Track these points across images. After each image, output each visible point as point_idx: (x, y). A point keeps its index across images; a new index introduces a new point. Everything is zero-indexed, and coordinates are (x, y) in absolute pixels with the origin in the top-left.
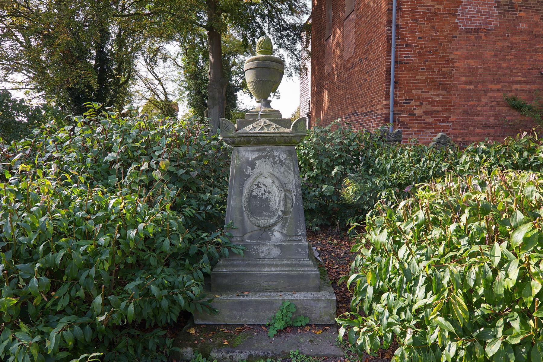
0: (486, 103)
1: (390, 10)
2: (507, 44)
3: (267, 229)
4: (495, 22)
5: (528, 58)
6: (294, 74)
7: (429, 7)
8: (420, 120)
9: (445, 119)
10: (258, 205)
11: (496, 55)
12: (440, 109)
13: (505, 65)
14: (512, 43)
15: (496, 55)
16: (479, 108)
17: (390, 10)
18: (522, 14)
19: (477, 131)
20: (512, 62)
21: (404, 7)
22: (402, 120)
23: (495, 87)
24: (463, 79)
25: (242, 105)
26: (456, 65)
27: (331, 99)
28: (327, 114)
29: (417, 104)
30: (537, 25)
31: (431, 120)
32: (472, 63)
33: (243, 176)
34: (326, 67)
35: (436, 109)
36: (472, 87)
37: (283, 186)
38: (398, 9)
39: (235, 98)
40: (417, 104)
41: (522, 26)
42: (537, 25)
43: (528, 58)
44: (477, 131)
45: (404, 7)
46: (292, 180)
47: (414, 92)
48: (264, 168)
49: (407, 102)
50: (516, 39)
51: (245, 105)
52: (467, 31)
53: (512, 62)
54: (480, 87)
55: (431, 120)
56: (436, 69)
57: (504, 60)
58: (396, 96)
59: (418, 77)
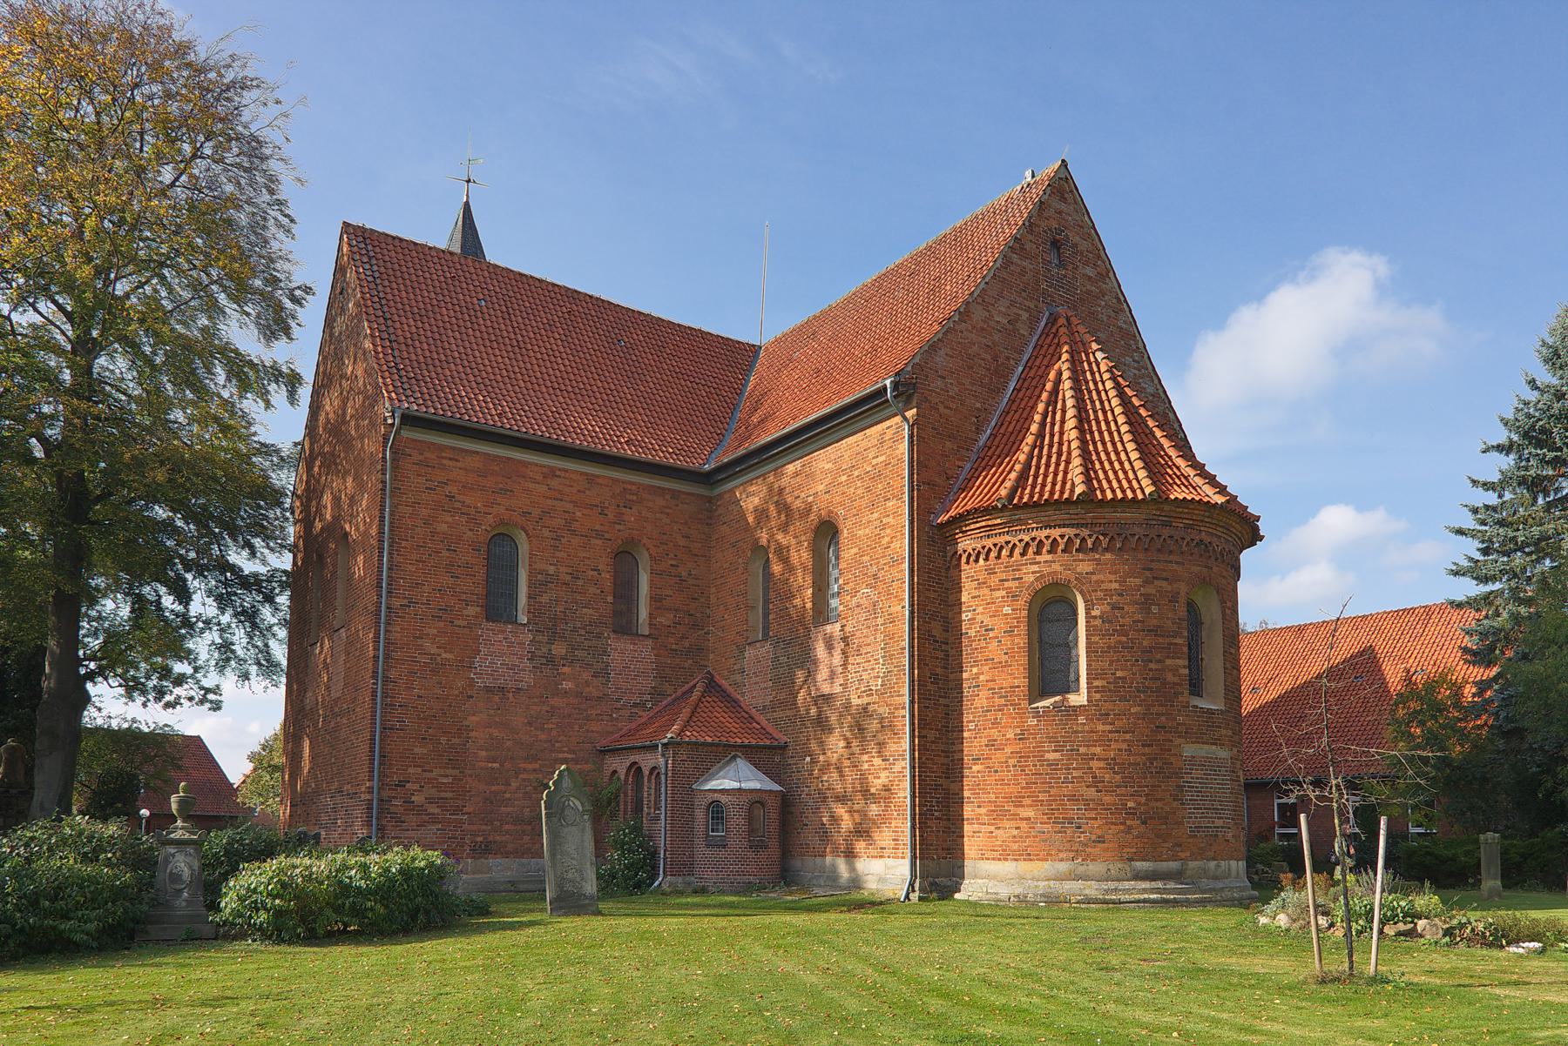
0: (518, 788)
1: (376, 658)
2: (545, 708)
3: (181, 891)
4: (528, 679)
5: (576, 728)
6: (253, 676)
7: (433, 656)
8: (420, 810)
9: (458, 810)
10: (175, 878)
11: (530, 724)
12: (449, 795)
13: (543, 737)
14: (553, 707)
15: (530, 724)
16: (507, 795)
17: (376, 658)
18: (566, 669)
19: (506, 827)
20: (554, 733)
21: (397, 655)
22: (392, 809)
23: (530, 766)
24: (483, 753)
25: (95, 714)
26: (473, 734)
27: (313, 757)
28: (306, 784)
29: (416, 787)
30: (587, 684)
31: (437, 811)
32: (496, 733)
33: (167, 861)
34: (309, 694)
35: (443, 795)
36: (496, 765)
37: (190, 867)
38: (387, 657)
39: (86, 699)
40: (416, 787)
41: (567, 685)
42: (587, 684)
43: (576, 728)
44: (506, 827)
45: (397, 655)
46: (196, 865)
47: (411, 770)
48: (180, 857)
49: (401, 784)
50: (558, 702)
51: (104, 713)
52: (488, 689)
53: (554, 733)
54: (507, 765)
55: (437, 811)
56: (443, 740)
57: (542, 729)
58: (382, 775)
59: (416, 750)
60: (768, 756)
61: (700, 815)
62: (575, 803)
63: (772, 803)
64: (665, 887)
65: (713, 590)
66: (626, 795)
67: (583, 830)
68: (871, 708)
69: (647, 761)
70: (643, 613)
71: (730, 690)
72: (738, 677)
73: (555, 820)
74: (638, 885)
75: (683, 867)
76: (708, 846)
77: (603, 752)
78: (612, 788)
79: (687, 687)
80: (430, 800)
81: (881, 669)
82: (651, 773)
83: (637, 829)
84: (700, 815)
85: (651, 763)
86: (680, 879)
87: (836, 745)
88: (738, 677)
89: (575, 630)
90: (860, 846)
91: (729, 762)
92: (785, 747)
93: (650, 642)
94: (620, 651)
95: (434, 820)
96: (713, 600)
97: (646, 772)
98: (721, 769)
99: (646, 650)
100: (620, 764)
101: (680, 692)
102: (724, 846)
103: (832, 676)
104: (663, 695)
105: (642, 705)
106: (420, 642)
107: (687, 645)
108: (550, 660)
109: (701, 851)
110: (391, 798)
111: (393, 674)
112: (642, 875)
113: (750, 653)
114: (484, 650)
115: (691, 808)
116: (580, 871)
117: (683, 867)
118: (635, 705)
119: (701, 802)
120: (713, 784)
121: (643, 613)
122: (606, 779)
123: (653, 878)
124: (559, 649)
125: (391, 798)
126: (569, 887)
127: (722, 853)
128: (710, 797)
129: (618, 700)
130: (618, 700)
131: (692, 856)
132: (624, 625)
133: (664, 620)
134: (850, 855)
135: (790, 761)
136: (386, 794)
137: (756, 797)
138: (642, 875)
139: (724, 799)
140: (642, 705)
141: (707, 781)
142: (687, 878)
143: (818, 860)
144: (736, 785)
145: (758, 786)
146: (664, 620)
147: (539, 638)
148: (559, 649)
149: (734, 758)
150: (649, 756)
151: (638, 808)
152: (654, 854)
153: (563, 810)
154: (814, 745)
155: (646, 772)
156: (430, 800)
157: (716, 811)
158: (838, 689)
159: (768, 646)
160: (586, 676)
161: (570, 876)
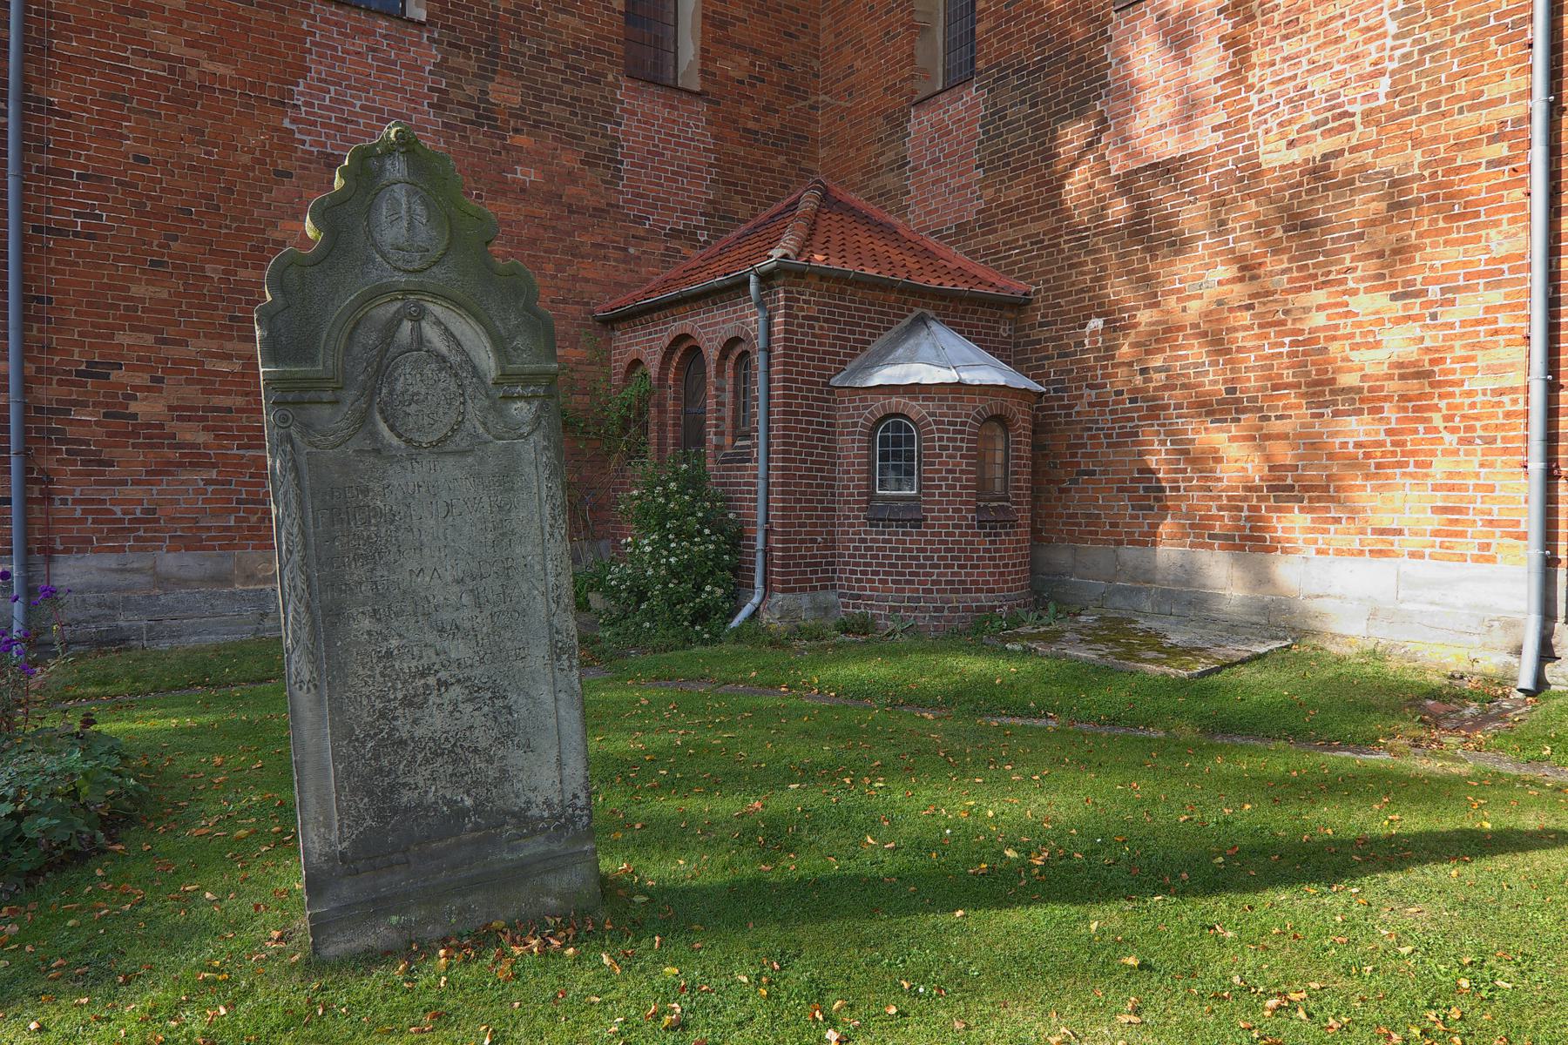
8: (154, 435)
18: (522, 140)
29: (142, 379)
30: (571, 177)
31: (202, 438)
35: (218, 400)
40: (142, 379)
41: (525, 174)
43: (550, 268)
47: (124, 338)
49: (95, 372)
55: (202, 438)
56: (213, 270)
59: (136, 290)
60: (985, 316)
61: (851, 449)
62: (457, 331)
63: (1022, 419)
64: (771, 619)
65: (825, 21)
66: (662, 410)
67: (507, 477)
68: (1340, 165)
69: (711, 329)
70: (689, 51)
71: (872, 208)
72: (890, 180)
73: (332, 418)
74: (701, 616)
75: (808, 569)
76: (873, 521)
77: (613, 322)
78: (631, 392)
79: (776, 207)
80: (183, 412)
81: (1390, 50)
82: (724, 355)
83: (694, 482)
84: (851, 449)
85: (728, 330)
86: (805, 600)
87: (1201, 279)
88: (890, 180)
89: (540, 56)
90: (1293, 523)
91: (910, 331)
92: (1019, 305)
93: (702, 107)
94: (639, 115)
95: (196, 458)
96: (827, 39)
97: (712, 353)
98: (895, 344)
99: (695, 124)
100: (646, 346)
101: (763, 215)
102: (918, 523)
103: (1189, 110)
104: (730, 218)
105: (689, 235)
106: (135, 23)
107: (776, 122)
108: (485, 115)
109: (854, 533)
110: (63, 409)
111: (57, 94)
112: (713, 591)
113: (920, 123)
114: (316, 69)
115: (827, 431)
116: (492, 693)
117: (808, 569)
118: (675, 234)
119: (852, 420)
120: (884, 376)
121: (689, 51)
122: (617, 380)
123: (735, 599)
124: (505, 94)
125: (63, 409)
126: (429, 786)
127: (912, 539)
128: (879, 405)
129: (640, 220)
130: (640, 220)
131: (830, 544)
132: (648, 62)
133: (733, 67)
134: (1251, 541)
135: (1036, 334)
136: (49, 393)
137: (992, 405)
138: (713, 591)
139: (916, 408)
140: (689, 235)
141: (880, 360)
142: (821, 596)
143: (1129, 553)
144: (949, 376)
145: (1000, 380)
146: (733, 67)
147: (457, 60)
148: (505, 94)
149: (921, 321)
150: (718, 315)
151: (692, 435)
152: (737, 539)
153: (382, 370)
154: (1118, 289)
155: (712, 353)
156: (183, 412)
157: (895, 433)
158: (1204, 138)
159: (971, 94)
160: (569, 160)
161: (435, 722)
